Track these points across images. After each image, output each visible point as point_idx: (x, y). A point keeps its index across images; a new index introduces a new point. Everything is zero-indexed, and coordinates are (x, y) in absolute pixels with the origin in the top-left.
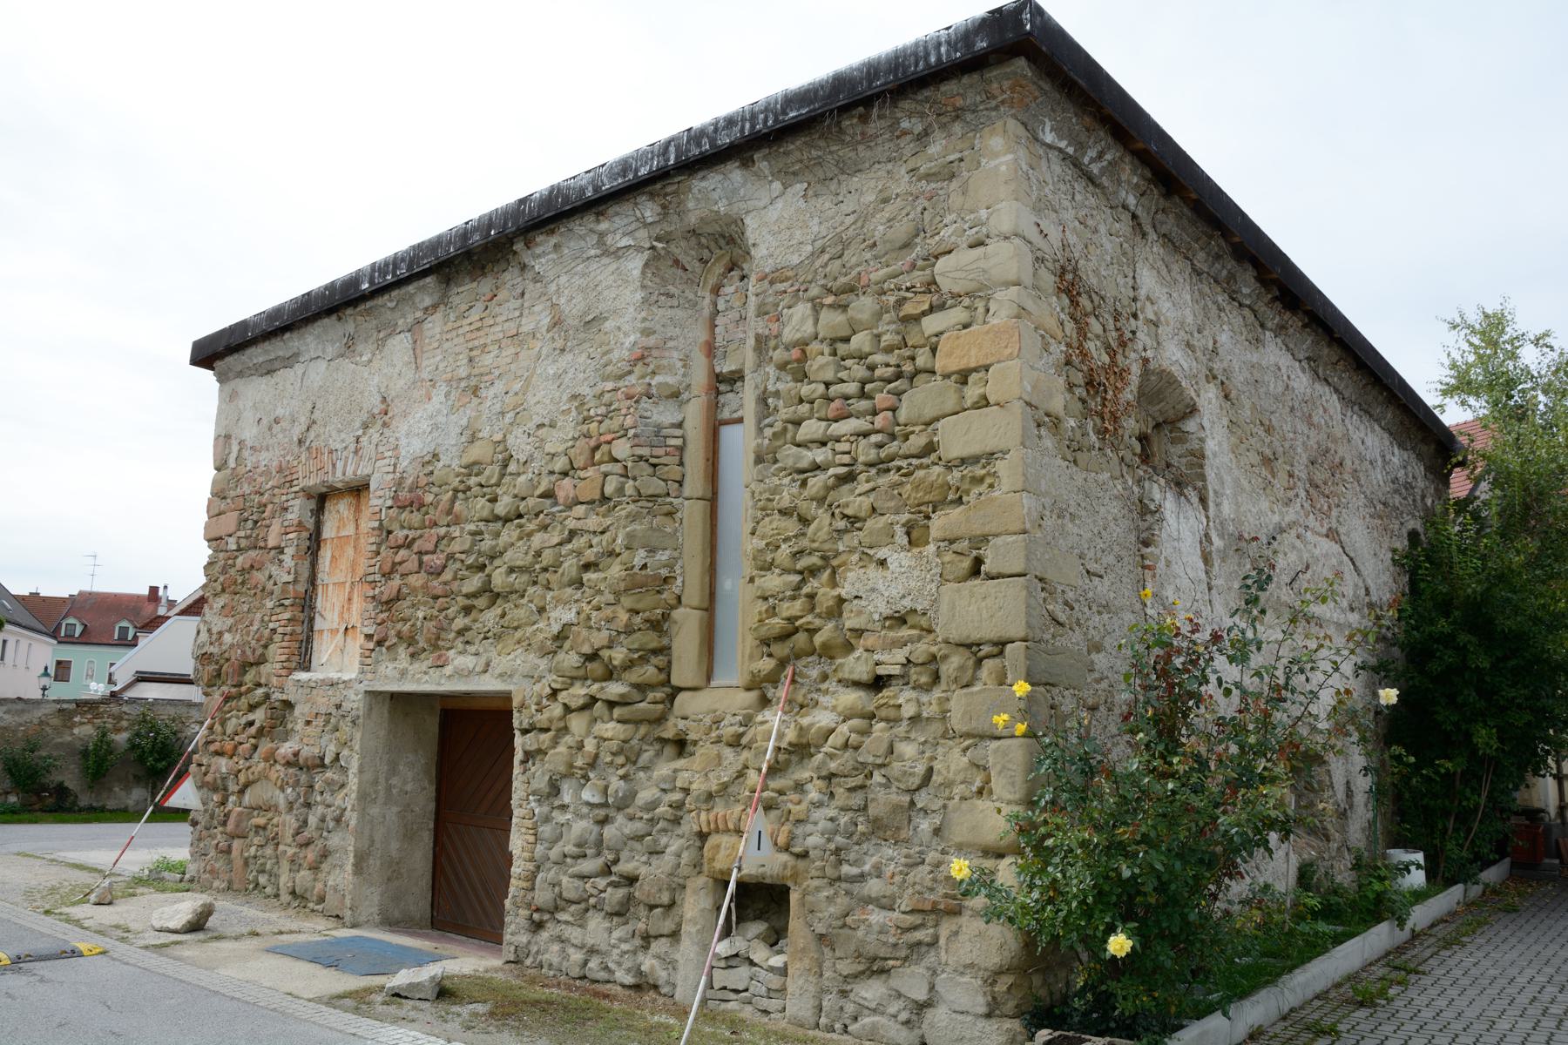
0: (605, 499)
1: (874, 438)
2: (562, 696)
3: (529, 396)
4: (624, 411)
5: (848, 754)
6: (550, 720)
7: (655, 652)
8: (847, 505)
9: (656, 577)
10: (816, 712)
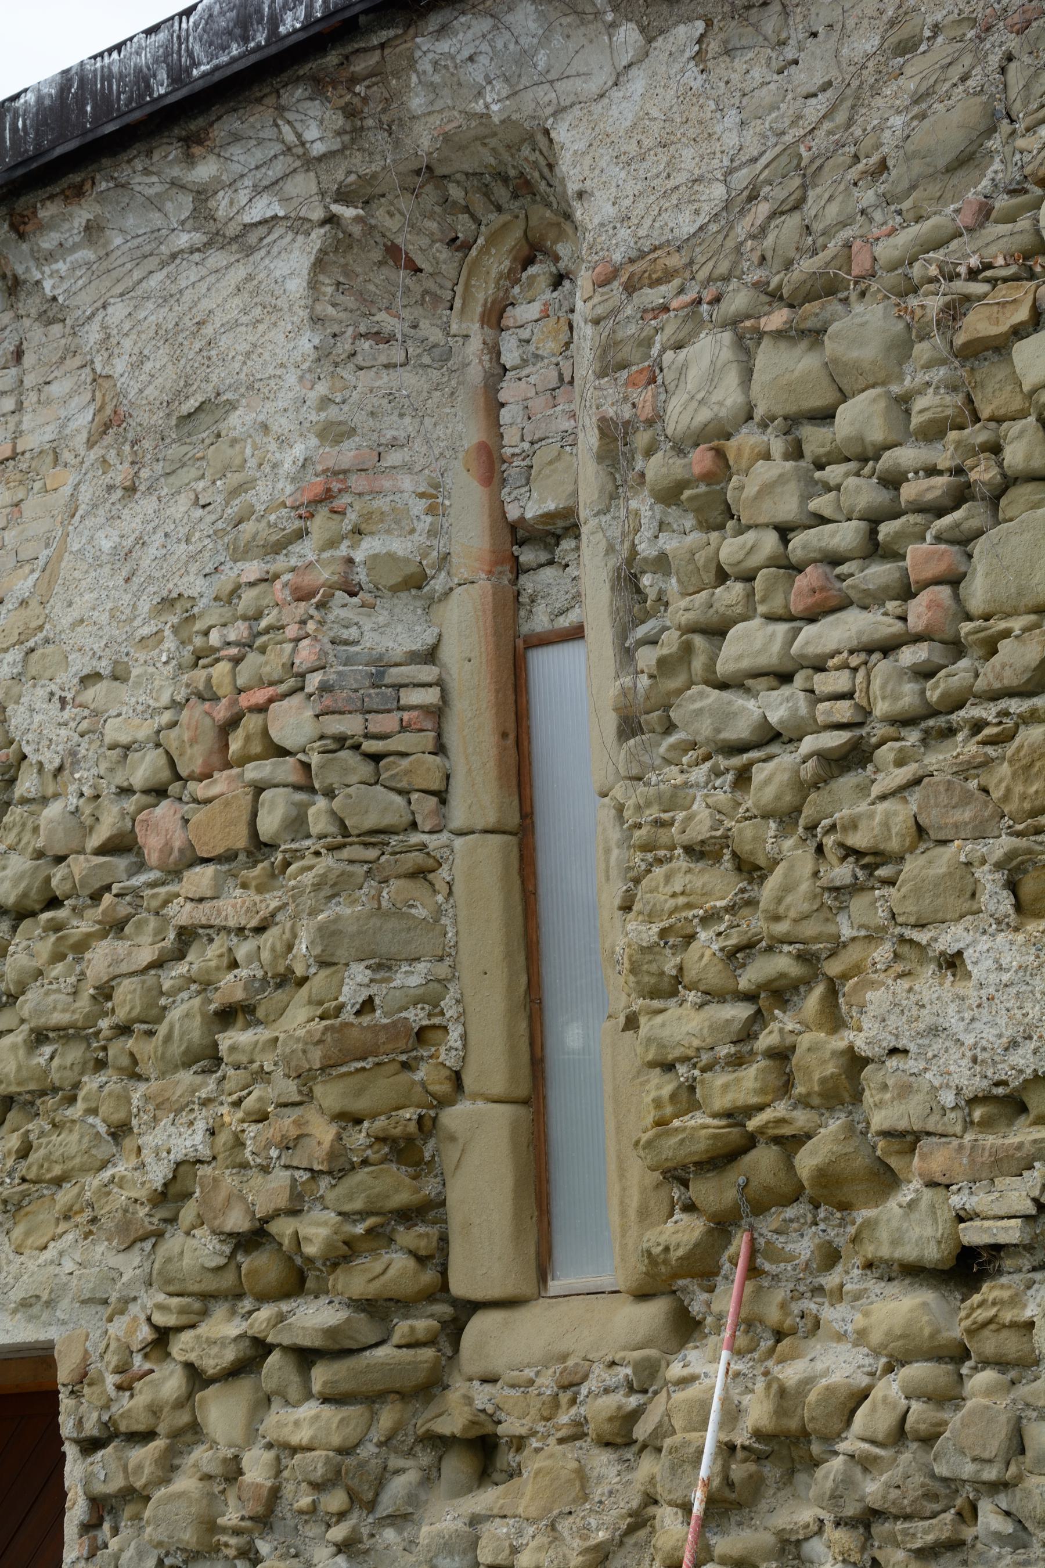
0: (259, 847)
1: (910, 656)
2: (182, 1346)
3: (56, 606)
4: (292, 631)
5: (908, 1456)
6: (155, 1410)
7: (408, 1215)
8: (853, 825)
9: (397, 1029)
10: (816, 1346)
